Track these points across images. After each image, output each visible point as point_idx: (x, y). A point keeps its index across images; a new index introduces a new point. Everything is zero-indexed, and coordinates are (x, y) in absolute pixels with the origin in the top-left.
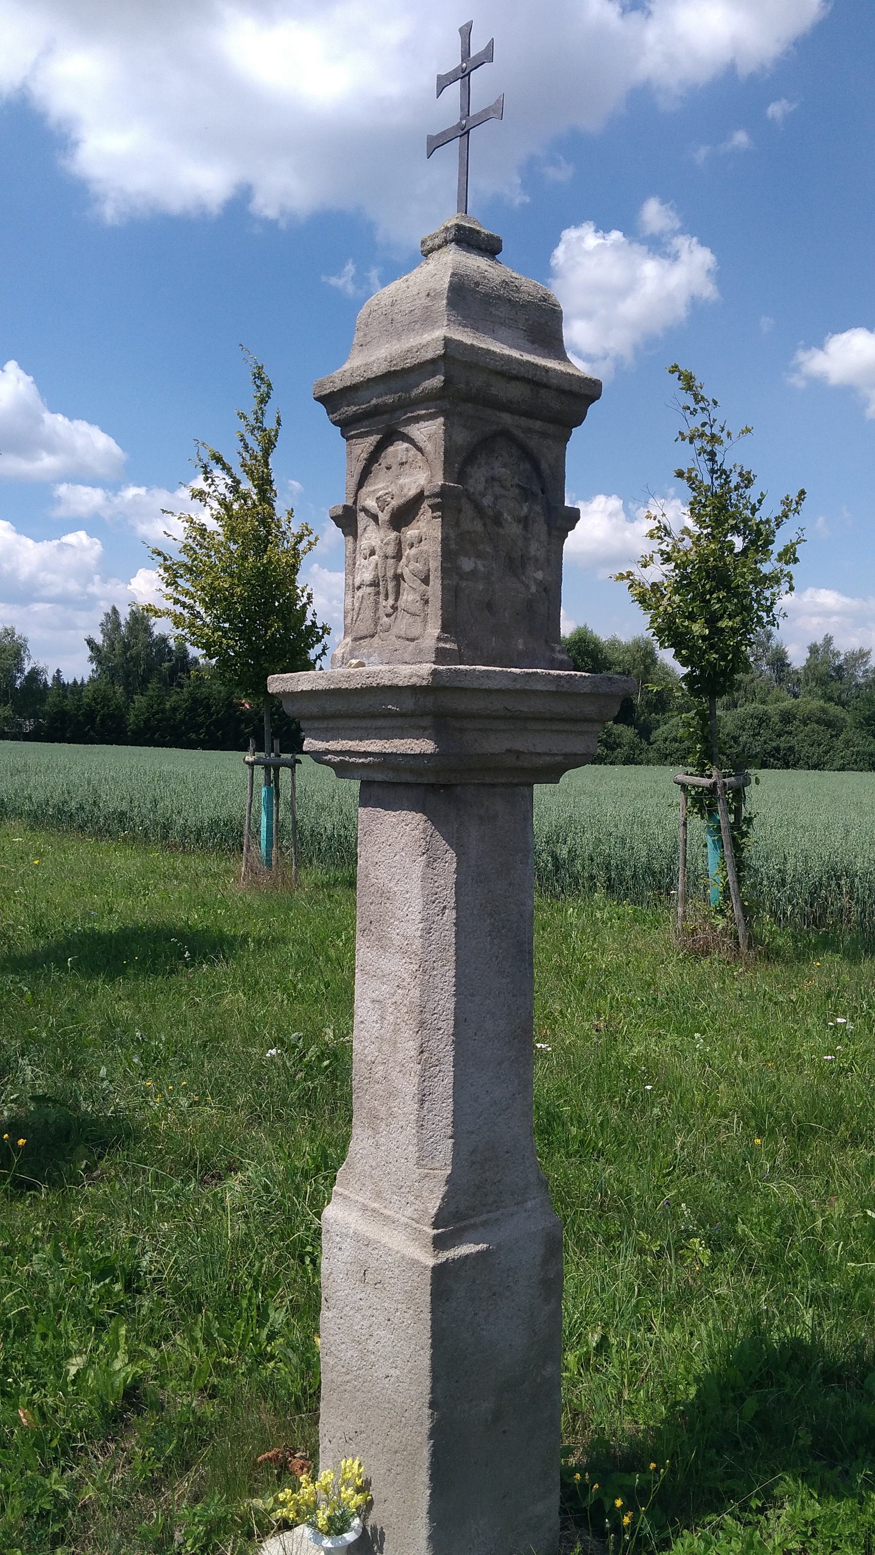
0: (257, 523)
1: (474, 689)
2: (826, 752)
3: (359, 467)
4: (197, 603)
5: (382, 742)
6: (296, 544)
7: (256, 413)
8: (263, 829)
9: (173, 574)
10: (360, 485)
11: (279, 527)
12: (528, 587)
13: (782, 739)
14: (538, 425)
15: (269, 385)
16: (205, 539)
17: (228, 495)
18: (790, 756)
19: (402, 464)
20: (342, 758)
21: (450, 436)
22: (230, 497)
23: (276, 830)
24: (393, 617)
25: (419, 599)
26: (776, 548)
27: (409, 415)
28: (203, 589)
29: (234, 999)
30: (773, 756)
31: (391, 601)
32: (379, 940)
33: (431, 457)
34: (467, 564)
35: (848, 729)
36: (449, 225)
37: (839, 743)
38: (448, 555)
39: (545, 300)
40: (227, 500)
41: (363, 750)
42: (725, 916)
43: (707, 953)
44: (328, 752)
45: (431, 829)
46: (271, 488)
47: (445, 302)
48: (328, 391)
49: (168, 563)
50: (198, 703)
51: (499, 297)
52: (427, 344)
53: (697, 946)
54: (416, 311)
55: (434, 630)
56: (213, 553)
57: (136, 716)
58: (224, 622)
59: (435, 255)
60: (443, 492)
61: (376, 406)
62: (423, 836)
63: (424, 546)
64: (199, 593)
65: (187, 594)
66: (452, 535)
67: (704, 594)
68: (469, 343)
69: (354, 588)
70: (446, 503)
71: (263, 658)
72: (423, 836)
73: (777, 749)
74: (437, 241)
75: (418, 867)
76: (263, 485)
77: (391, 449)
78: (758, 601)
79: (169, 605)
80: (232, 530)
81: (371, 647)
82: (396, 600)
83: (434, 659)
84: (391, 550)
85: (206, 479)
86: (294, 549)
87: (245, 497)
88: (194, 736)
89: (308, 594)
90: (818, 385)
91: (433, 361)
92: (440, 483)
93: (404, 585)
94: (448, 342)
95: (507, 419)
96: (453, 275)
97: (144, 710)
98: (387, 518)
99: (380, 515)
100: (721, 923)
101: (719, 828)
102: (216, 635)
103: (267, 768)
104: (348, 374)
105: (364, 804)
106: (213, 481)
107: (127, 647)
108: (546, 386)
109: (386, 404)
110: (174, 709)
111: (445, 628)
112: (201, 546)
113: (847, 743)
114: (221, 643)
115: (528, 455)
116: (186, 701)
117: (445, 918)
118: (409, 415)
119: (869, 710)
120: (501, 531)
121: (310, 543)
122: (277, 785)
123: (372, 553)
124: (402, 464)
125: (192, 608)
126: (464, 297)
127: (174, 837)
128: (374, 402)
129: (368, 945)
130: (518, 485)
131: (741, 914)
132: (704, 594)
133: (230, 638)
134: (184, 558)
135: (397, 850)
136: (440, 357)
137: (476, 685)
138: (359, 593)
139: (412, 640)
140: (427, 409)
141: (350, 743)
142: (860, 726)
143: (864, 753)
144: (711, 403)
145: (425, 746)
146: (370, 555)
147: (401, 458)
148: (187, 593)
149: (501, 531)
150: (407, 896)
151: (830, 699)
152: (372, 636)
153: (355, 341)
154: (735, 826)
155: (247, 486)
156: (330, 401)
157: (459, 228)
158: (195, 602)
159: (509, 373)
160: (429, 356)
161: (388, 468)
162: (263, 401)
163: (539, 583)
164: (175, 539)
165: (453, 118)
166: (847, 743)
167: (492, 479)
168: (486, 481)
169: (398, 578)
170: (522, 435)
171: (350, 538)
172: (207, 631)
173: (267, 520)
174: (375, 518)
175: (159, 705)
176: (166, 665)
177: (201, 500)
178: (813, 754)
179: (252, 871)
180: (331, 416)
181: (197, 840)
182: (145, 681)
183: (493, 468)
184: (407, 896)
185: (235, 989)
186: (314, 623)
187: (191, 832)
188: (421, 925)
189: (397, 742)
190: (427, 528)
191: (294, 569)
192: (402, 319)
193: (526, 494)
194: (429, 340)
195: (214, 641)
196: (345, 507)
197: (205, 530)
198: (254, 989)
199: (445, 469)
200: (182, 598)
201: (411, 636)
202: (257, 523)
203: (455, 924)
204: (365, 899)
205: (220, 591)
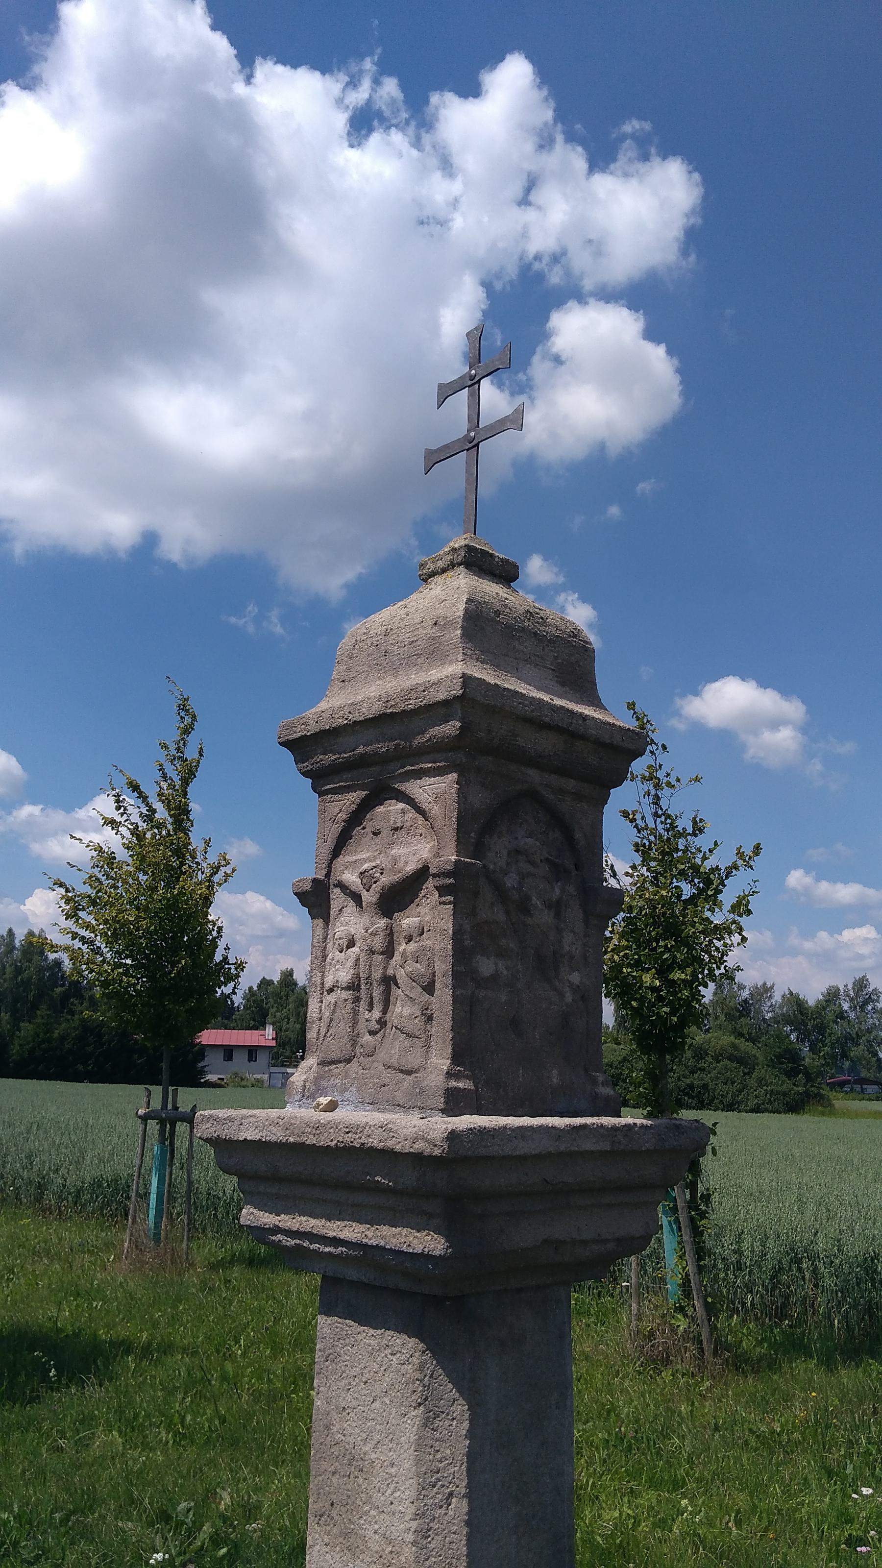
0: (170, 853)
1: (504, 1158)
2: (740, 1091)
3: (335, 830)
4: (99, 938)
5: (362, 1227)
6: (211, 875)
7: (178, 743)
8: (153, 1196)
9: (74, 907)
10: (336, 852)
11: (194, 858)
12: (562, 995)
13: (696, 1076)
14: (571, 784)
15: (194, 717)
16: (113, 869)
17: (141, 824)
18: (704, 1094)
19: (396, 829)
20: (298, 1242)
21: (465, 797)
22: (143, 826)
23: (168, 1196)
24: (379, 1036)
25: (419, 1013)
26: (728, 897)
27: (408, 768)
28: (106, 922)
29: (107, 1439)
30: (687, 1094)
31: (376, 1014)
32: (346, 1535)
33: (438, 823)
34: (486, 966)
35: (760, 1066)
36: (457, 546)
37: (752, 1082)
38: (463, 953)
39: (575, 636)
40: (140, 829)
41: (331, 1234)
42: (685, 1316)
43: (667, 1362)
44: (277, 1230)
45: (431, 1365)
46: (188, 818)
47: (459, 632)
48: (299, 735)
49: (70, 894)
50: (89, 1030)
51: (523, 630)
52: (439, 683)
53: (656, 1352)
54: (419, 643)
55: (440, 1061)
56: (120, 884)
57: (21, 1045)
58: (126, 957)
59: (438, 579)
60: (457, 870)
61: (362, 755)
62: (418, 1375)
63: (427, 941)
64: (101, 927)
65: (87, 927)
66: (467, 927)
67: (649, 942)
68: (493, 682)
69: (322, 989)
70: (459, 885)
71: (167, 998)
72: (418, 1375)
73: (691, 1086)
74: (440, 564)
75: (409, 1427)
76: (179, 814)
77: (380, 809)
78: (708, 952)
79: (66, 940)
80: (142, 858)
81: (346, 1077)
82: (385, 1011)
83: (442, 1106)
84: (379, 943)
85: (118, 808)
86: (209, 881)
87: (160, 826)
88: (80, 1067)
89: (218, 927)
90: (699, 729)
91: (446, 703)
92: (453, 858)
93: (396, 992)
94: (466, 679)
95: (534, 776)
96: (469, 601)
97: (30, 1039)
98: (374, 900)
99: (365, 896)
100: (682, 1324)
101: (676, 1206)
102: (116, 972)
103: (162, 1123)
104: (326, 715)
105: (328, 1309)
106: (125, 809)
107: (18, 971)
108: (583, 737)
109: (376, 754)
110: (63, 1038)
111: (456, 1059)
112: (108, 875)
113: (761, 1082)
114: (121, 981)
115: (560, 822)
116: (75, 1029)
117: (451, 1513)
118: (408, 768)
119: (780, 1048)
120: (529, 921)
121: (227, 875)
122: (172, 1144)
123: (351, 944)
124: (396, 829)
125: (91, 942)
126: (481, 627)
127: (50, 1199)
128: (361, 750)
129: (326, 1540)
130: (547, 859)
131: (704, 1314)
132: (649, 942)
133: (132, 976)
134: (88, 890)
135: (378, 1391)
136: (456, 698)
137: (507, 1150)
138: (331, 998)
139: (409, 1073)
140: (435, 763)
141: (313, 1222)
142: (771, 1064)
143: (778, 1093)
144: (660, 747)
145: (428, 1242)
146: (348, 947)
147: (395, 822)
148: (88, 926)
149: (529, 921)
150: (393, 1471)
151: (741, 1035)
152: (349, 1061)
153: (335, 675)
154: (692, 1204)
155: (162, 813)
156: (300, 747)
157: (469, 549)
158: (96, 936)
159: (540, 720)
160: (442, 696)
161: (376, 834)
162: (187, 731)
163: (575, 989)
164: (79, 870)
165: (461, 428)
166: (761, 1082)
167: (516, 853)
168: (509, 854)
169: (389, 981)
170: (551, 797)
171: (320, 922)
172: (107, 968)
173: (181, 851)
174: (357, 898)
175: (45, 1034)
176: (58, 990)
177: (113, 829)
178: (728, 1093)
179: (137, 1247)
180: (300, 765)
181: (76, 1204)
182: (35, 1007)
183: (517, 838)
184: (393, 1471)
185: (109, 1428)
186: (225, 959)
187: (69, 1193)
188: (414, 1525)
189: (386, 1230)
190: (430, 919)
191: (207, 901)
192: (408, 649)
193: (558, 872)
194: (446, 674)
195: (113, 979)
196: (315, 881)
197: (115, 858)
198: (132, 1427)
199: (458, 840)
200: (82, 932)
201: (407, 1066)
202: (170, 853)
203: (468, 1523)
204: (324, 1465)
205: (123, 926)
